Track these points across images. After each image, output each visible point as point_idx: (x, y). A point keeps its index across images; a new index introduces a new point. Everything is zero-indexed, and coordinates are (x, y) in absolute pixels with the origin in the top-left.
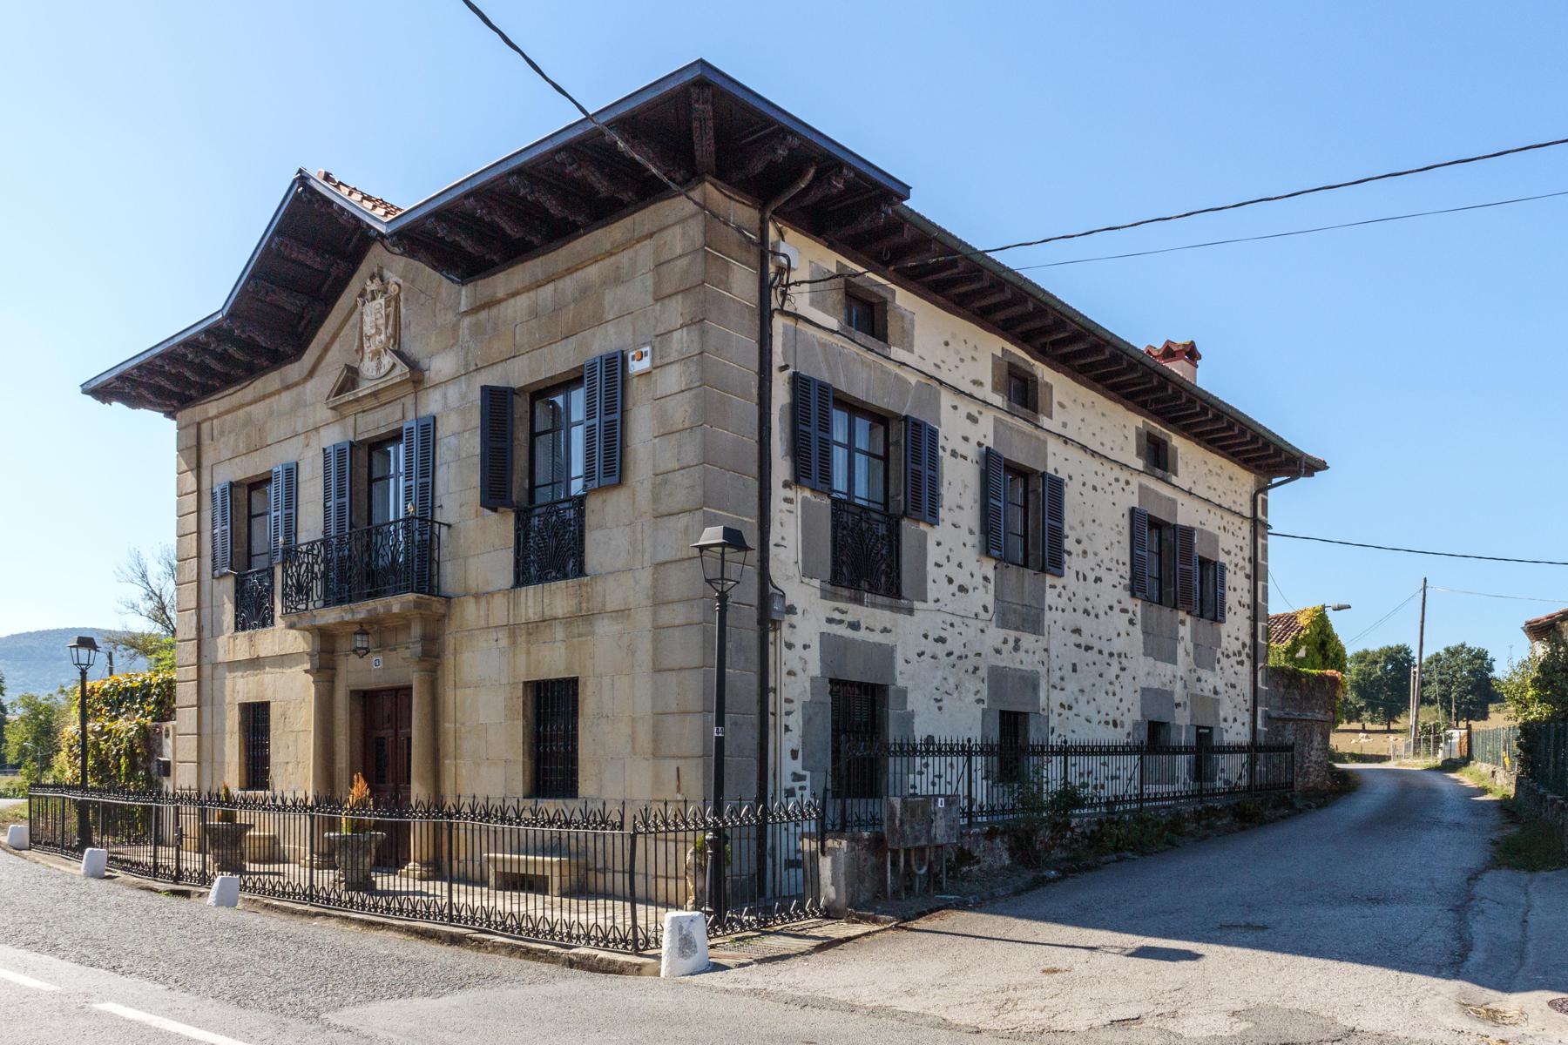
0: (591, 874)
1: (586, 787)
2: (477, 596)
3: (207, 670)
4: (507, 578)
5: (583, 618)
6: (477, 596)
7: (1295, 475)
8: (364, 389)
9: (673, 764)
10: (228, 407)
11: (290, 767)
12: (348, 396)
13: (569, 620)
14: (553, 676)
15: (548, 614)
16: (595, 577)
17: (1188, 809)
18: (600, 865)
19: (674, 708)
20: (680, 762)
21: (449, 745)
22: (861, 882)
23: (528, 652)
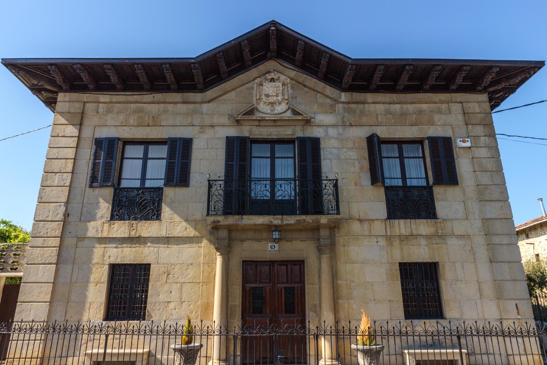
0: (511, 358)
1: (450, 311)
2: (361, 221)
3: (70, 241)
4: (385, 215)
5: (440, 237)
6: (361, 221)
7: (540, 68)
8: (258, 115)
9: (513, 303)
10: (123, 100)
11: (172, 305)
12: (246, 117)
13: (428, 237)
14: (420, 261)
15: (415, 232)
16: (444, 220)
17: (529, 233)
18: (484, 351)
19: (509, 278)
20: (517, 302)
21: (344, 292)
22: (144, 279)
23: (401, 249)
